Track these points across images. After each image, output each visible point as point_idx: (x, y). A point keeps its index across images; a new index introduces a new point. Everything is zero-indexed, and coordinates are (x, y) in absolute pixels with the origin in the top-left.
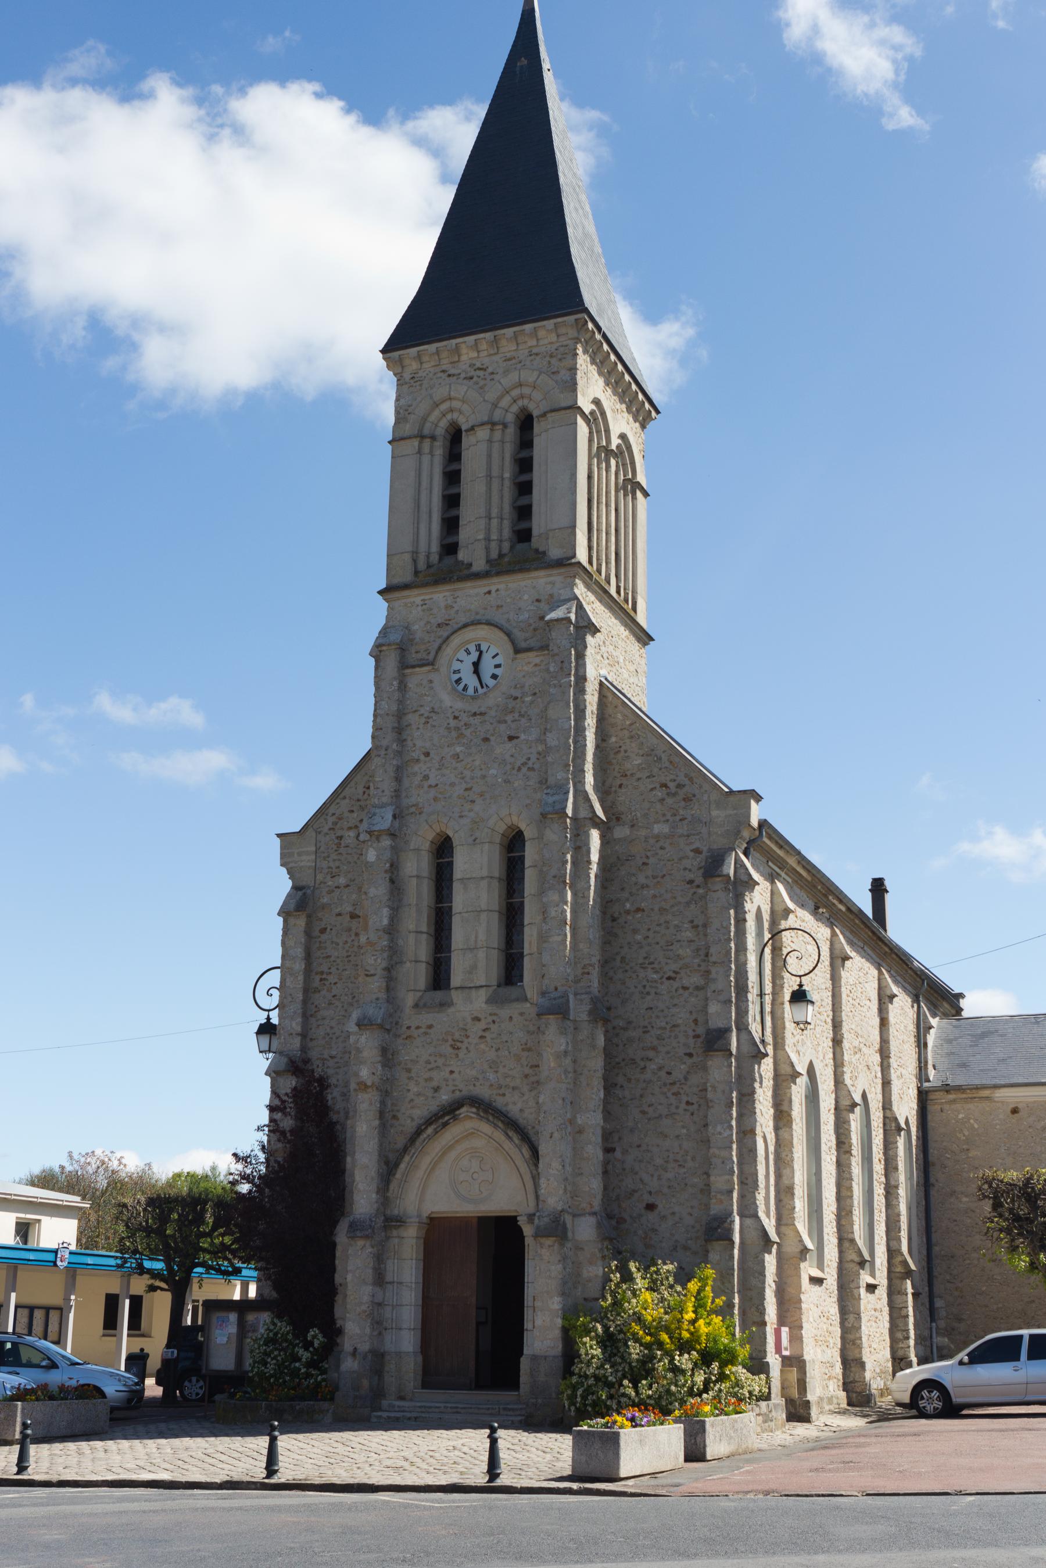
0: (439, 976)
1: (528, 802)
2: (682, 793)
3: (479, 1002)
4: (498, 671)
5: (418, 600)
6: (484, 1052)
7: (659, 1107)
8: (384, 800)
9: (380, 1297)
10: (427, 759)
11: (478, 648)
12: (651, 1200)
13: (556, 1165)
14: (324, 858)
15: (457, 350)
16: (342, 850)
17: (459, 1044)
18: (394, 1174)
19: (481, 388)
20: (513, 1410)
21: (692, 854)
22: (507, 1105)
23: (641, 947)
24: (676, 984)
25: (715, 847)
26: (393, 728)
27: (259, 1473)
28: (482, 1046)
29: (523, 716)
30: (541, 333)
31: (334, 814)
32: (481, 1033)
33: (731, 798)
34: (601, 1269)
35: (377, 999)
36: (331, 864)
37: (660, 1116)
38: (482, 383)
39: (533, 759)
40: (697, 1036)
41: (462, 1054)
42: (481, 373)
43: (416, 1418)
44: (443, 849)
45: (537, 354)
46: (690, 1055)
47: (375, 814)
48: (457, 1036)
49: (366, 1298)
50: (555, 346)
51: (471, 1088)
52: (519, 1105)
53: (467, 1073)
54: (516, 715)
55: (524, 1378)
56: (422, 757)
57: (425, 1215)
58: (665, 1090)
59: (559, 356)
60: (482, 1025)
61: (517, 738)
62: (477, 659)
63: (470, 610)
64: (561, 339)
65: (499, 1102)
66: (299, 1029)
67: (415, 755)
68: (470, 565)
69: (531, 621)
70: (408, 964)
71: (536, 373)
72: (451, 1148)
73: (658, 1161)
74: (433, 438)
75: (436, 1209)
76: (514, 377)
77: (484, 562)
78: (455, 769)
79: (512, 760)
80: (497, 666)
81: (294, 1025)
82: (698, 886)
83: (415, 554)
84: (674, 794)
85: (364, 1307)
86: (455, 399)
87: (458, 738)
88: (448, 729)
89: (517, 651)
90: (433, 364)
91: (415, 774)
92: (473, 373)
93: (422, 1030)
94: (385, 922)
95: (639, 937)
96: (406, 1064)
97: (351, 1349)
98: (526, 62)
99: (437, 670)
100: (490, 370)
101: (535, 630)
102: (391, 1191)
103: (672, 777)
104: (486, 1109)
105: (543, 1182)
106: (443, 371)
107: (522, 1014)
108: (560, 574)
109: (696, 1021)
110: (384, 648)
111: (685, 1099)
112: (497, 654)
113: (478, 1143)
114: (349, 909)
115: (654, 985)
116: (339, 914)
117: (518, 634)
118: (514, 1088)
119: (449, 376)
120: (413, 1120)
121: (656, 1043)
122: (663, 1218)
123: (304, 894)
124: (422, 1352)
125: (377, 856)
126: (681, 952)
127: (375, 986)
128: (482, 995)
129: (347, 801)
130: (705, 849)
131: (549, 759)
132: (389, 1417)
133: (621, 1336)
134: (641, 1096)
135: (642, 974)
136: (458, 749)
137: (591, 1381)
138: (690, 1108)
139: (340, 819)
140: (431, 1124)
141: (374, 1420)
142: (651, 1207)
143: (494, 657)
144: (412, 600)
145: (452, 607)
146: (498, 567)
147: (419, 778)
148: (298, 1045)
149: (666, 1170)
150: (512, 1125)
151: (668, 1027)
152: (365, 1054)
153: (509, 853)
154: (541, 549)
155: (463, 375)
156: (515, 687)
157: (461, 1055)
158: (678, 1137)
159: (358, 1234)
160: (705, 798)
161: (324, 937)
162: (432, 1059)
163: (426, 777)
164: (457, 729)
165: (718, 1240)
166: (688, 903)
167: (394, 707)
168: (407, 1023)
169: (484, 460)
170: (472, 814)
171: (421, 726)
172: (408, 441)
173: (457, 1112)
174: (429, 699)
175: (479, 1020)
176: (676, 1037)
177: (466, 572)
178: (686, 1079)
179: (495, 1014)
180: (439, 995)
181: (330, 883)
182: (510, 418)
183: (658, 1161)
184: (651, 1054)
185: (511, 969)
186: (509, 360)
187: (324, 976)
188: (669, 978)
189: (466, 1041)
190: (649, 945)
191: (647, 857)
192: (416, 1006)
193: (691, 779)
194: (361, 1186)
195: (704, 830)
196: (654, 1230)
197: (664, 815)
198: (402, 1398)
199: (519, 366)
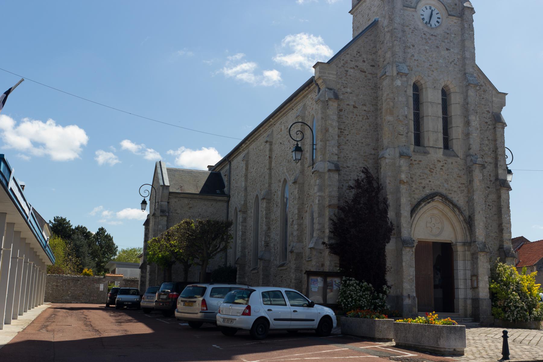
0: (418, 141)
4: (439, 20)
9: (405, 275)
13: (481, 224)
14: (340, 78)
16: (347, 77)
21: (486, 112)
31: (343, 60)
33: (499, 95)
36: (343, 82)
39: (456, 60)
40: (491, 181)
41: (434, 174)
44: (417, 88)
46: (489, 188)
48: (431, 167)
53: (436, 182)
56: (411, 46)
60: (441, 164)
65: (450, 196)
81: (334, 150)
85: (411, 277)
88: (422, 37)
89: (449, 15)
93: (416, 162)
99: (416, 11)
101: (453, 8)
104: (446, 199)
107: (456, 162)
109: (490, 175)
111: (488, 204)
113: (435, 212)
116: (348, 105)
118: (455, 192)
123: (334, 92)
125: (402, 84)
126: (484, 148)
129: (349, 56)
130: (491, 112)
136: (427, 48)
139: (347, 63)
150: (454, 206)
153: (418, 95)
157: (433, 175)
160: (490, 92)
162: (422, 175)
163: (413, 56)
194: (404, 225)
195: (490, 104)
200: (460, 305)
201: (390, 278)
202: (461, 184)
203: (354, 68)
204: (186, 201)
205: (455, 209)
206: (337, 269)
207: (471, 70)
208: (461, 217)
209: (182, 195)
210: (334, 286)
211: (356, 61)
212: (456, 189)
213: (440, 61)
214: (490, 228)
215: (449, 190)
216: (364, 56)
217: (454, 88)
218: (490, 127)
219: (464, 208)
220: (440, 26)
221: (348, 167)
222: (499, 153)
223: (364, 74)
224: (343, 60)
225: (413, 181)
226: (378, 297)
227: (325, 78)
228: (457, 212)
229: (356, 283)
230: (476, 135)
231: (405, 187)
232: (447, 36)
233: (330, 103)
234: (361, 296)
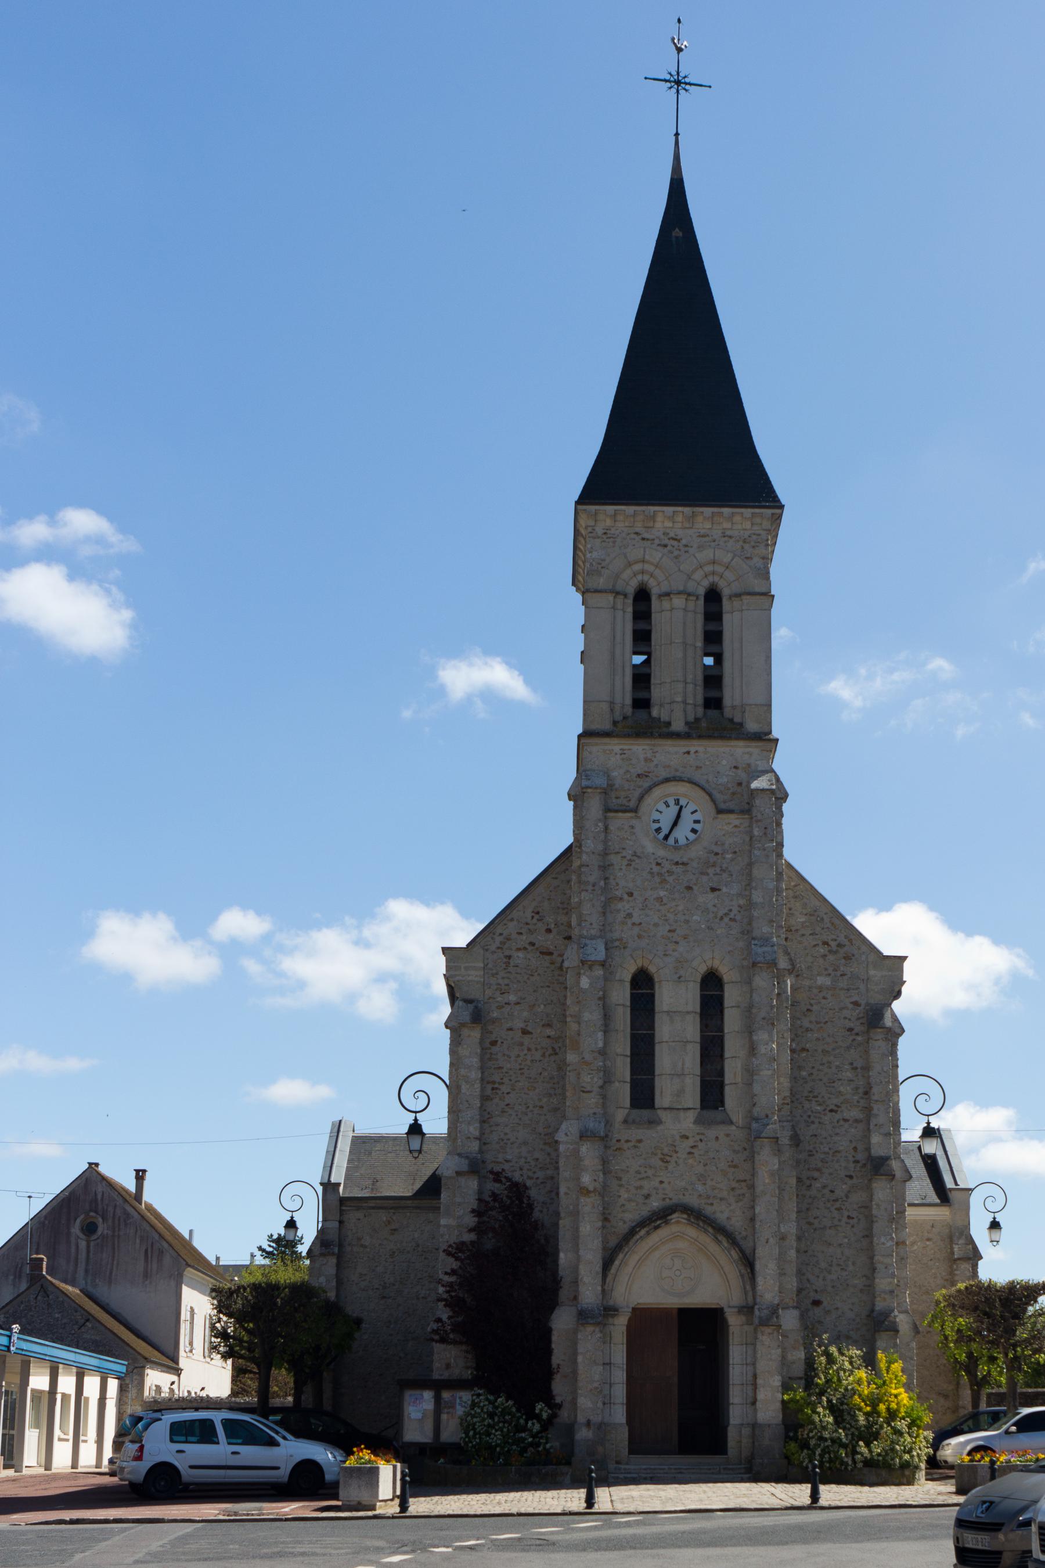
0: (643, 1095)
1: (730, 948)
2: (842, 951)
3: (687, 1122)
4: (697, 826)
5: (617, 749)
8: (593, 932)
9: (595, 1377)
10: (631, 899)
11: (677, 802)
12: (818, 1297)
14: (493, 975)
15: (653, 518)
16: (510, 969)
17: (668, 1158)
19: (676, 557)
20: (732, 1469)
21: (851, 1006)
22: (714, 1213)
23: (806, 1082)
24: (838, 1116)
25: (872, 1001)
26: (599, 866)
27: (807, 1501)
28: (690, 1161)
29: (724, 871)
30: (737, 519)
31: (501, 934)
32: (689, 1150)
35: (595, 1114)
36: (501, 981)
37: (825, 1228)
38: (676, 553)
39: (735, 910)
41: (670, 1167)
42: (675, 543)
44: (643, 985)
45: (730, 537)
46: (851, 1177)
47: (586, 945)
48: (666, 1151)
49: (597, 1377)
50: (747, 533)
51: (681, 1197)
53: (678, 1183)
54: (718, 870)
56: (626, 896)
57: (632, 1305)
58: (829, 1205)
59: (753, 544)
60: (690, 1142)
61: (719, 890)
62: (678, 814)
63: (669, 766)
64: (755, 528)
65: (708, 1210)
66: (477, 1133)
67: (618, 893)
68: (669, 724)
69: (730, 785)
70: (617, 1084)
71: (730, 555)
73: (823, 1265)
74: (625, 596)
75: (640, 1301)
76: (707, 554)
77: (683, 724)
78: (659, 911)
79: (715, 910)
80: (697, 822)
81: (471, 1129)
82: (857, 1034)
83: (612, 703)
84: (836, 952)
85: (596, 1385)
86: (648, 562)
87: (661, 883)
89: (720, 811)
90: (627, 524)
91: (618, 911)
92: (666, 541)
93: (630, 1144)
94: (601, 1044)
95: (804, 1073)
98: (681, 234)
100: (684, 542)
101: (734, 794)
103: (834, 937)
104: (696, 1216)
105: (760, 1280)
106: (637, 533)
107: (728, 1135)
108: (756, 747)
109: (855, 1149)
110: (589, 790)
111: (846, 1214)
112: (696, 811)
114: (522, 1025)
116: (511, 1029)
117: (718, 796)
118: (721, 1199)
119: (643, 539)
120: (625, 1223)
121: (820, 1165)
122: (828, 1312)
123: (476, 1007)
125: (591, 984)
126: (842, 1089)
127: (592, 1101)
128: (691, 1116)
129: (515, 923)
130: (863, 1003)
131: (755, 914)
133: (845, 1407)
134: (808, 1209)
135: (807, 1105)
136: (662, 893)
137: (829, 1443)
138: (851, 1221)
142: (817, 1303)
143: (692, 813)
144: (610, 747)
145: (651, 761)
146: (694, 731)
147: (622, 915)
148: (477, 1148)
149: (830, 1272)
150: (720, 1230)
151: (831, 1152)
152: (587, 1162)
154: (737, 720)
155: (657, 542)
156: (716, 844)
158: (840, 1245)
161: (495, 1049)
163: (629, 915)
164: (660, 874)
165: (887, 1330)
166: (848, 1048)
167: (600, 847)
168: (617, 1136)
169: (676, 623)
170: (675, 953)
171: (624, 867)
172: (604, 595)
174: (631, 843)
175: (687, 1138)
176: (838, 1161)
177: (665, 730)
178: (847, 1197)
179: (703, 1134)
180: (645, 1113)
181: (499, 999)
182: (701, 591)
183: (823, 1265)
184: (816, 1174)
185: (712, 1094)
186: (703, 536)
187: (496, 1086)
188: (831, 1111)
189: (675, 1155)
190: (813, 1080)
191: (811, 1005)
192: (625, 1121)
193: (850, 941)
194: (586, 1280)
195: (862, 987)
196: (820, 1322)
197: (826, 969)
198: (618, 1463)
199: (713, 544)
200: (730, 1439)
201: (559, 1387)
202: (738, 1181)
203: (525, 949)
204: (383, 1215)
205: (720, 1238)
206: (468, 1374)
207: (766, 929)
208: (733, 1252)
209: (372, 1204)
210: (458, 1407)
211: (531, 932)
213: (695, 918)
214: (851, 1268)
215: (708, 1197)
216: (550, 919)
217: (728, 974)
218: (859, 1038)
219: (744, 1233)
220: (696, 840)
221: (507, 1161)
222: (875, 1098)
223: (547, 957)
224: (501, 934)
225: (621, 1186)
226: (524, 1429)
227: (457, 978)
229: (487, 1399)
230: (770, 1072)
231: (588, 1200)
232: (713, 859)
233: (465, 1032)
234: (489, 1425)
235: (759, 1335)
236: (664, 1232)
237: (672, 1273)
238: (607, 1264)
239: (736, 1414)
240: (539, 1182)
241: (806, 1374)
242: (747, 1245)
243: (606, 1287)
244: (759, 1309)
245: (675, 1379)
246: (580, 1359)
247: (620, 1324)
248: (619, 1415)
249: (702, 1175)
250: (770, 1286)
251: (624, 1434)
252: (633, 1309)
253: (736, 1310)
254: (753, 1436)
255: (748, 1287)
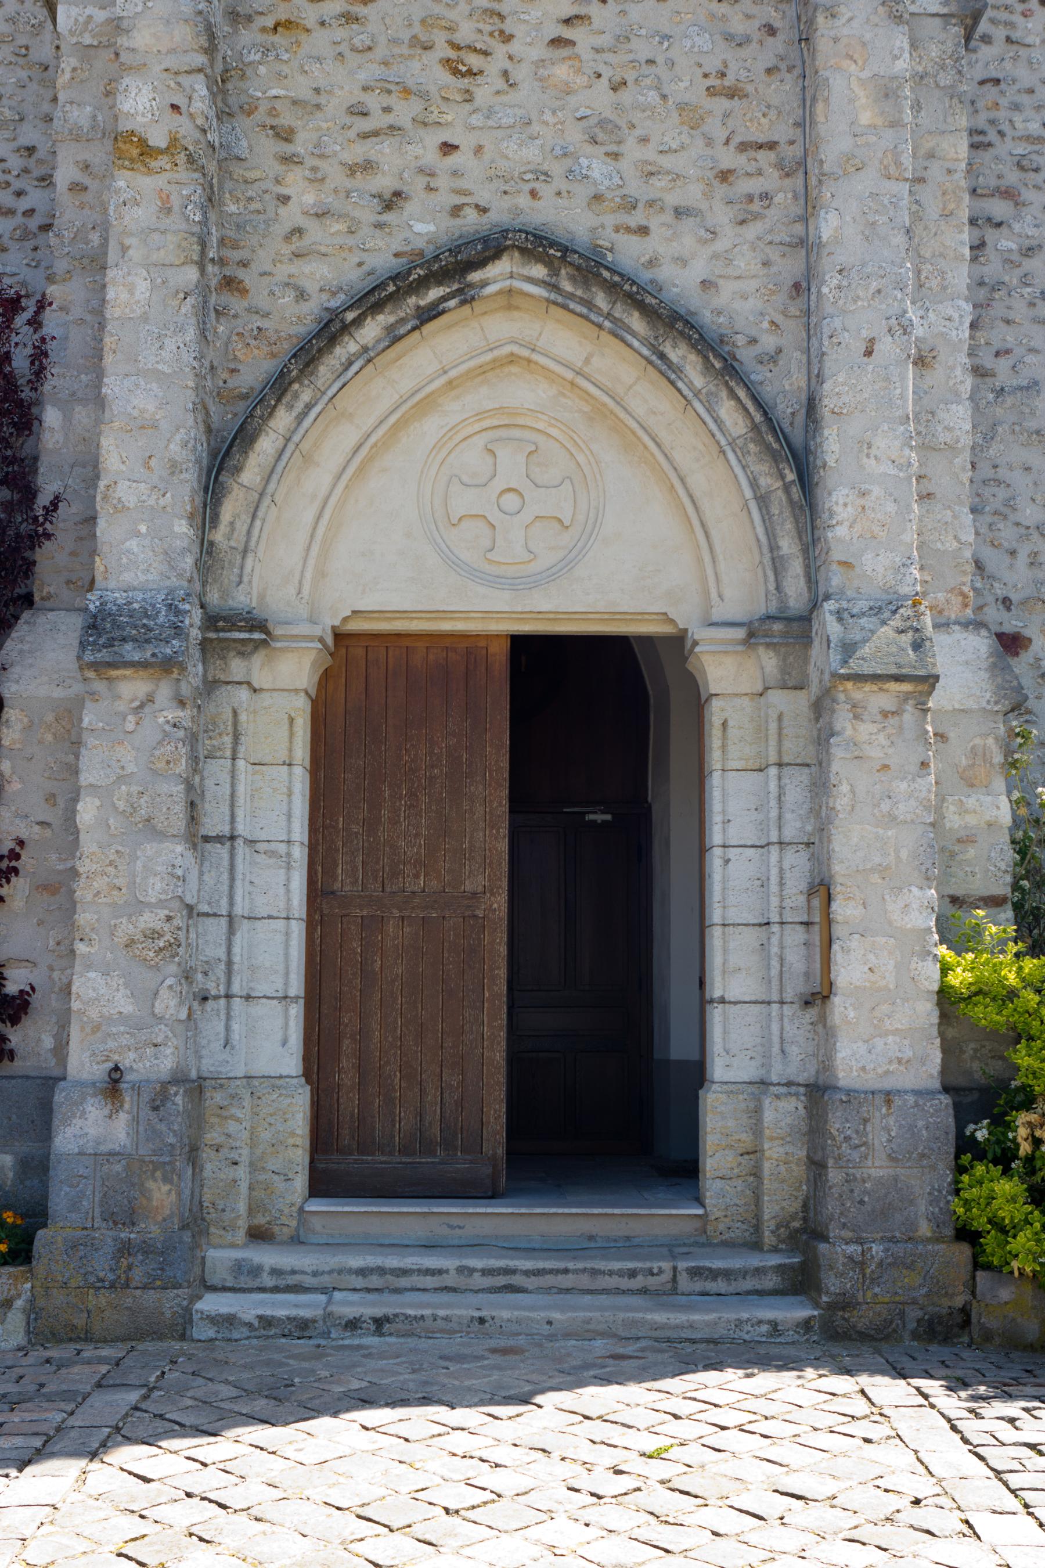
6: (569, 91)
7: (1030, 359)
12: (1011, 624)
17: (474, 61)
18: (238, 469)
22: (652, 263)
28: (561, 72)
34: (1004, 802)
41: (483, 94)
43: (379, 1323)
48: (466, 33)
49: (155, 888)
52: (698, 269)
55: (717, 1157)
57: (331, 620)
65: (629, 253)
72: (424, 405)
85: (149, 920)
96: (272, 112)
97: (98, 1071)
102: (223, 528)
105: (840, 502)
113: (523, 393)
115: (1003, 15)
118: (679, 212)
121: (1013, 177)
124: (307, 1074)
132: (266, 1322)
140: (377, 307)
141: (203, 1331)
159: (130, 652)
162: (373, 102)
173: (475, 276)
189: (501, 51)
194: (126, 493)
198: (258, 1235)
202: (744, 147)
205: (677, 352)
208: (727, 410)
212: (692, 194)
219: (769, 342)
225: (288, 160)
228: (694, 372)
235: (843, 720)
236: (452, 343)
237: (479, 499)
238: (222, 456)
239: (738, 1039)
240: (33, 224)
241: (1016, 887)
242: (784, 387)
243: (218, 536)
244: (839, 616)
245: (500, 902)
246: (87, 811)
247: (277, 700)
248: (269, 1041)
249: (602, 123)
250: (891, 517)
251: (291, 1116)
252: (339, 636)
253: (740, 633)
254: (815, 1129)
255: (788, 545)
